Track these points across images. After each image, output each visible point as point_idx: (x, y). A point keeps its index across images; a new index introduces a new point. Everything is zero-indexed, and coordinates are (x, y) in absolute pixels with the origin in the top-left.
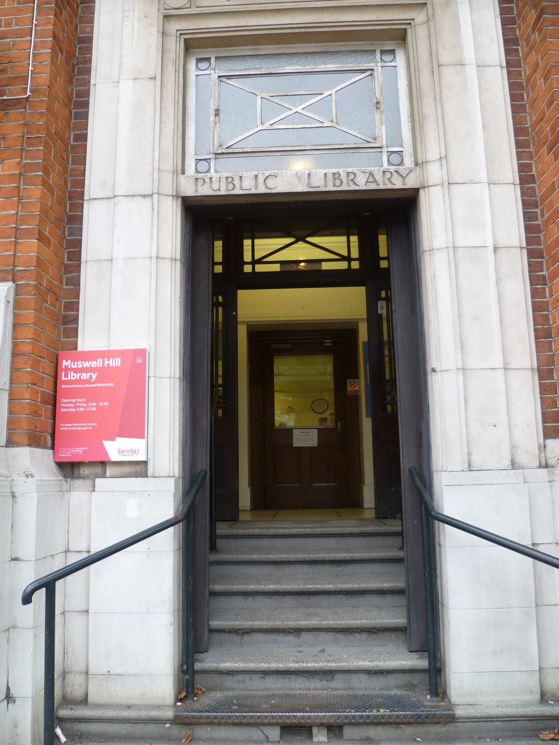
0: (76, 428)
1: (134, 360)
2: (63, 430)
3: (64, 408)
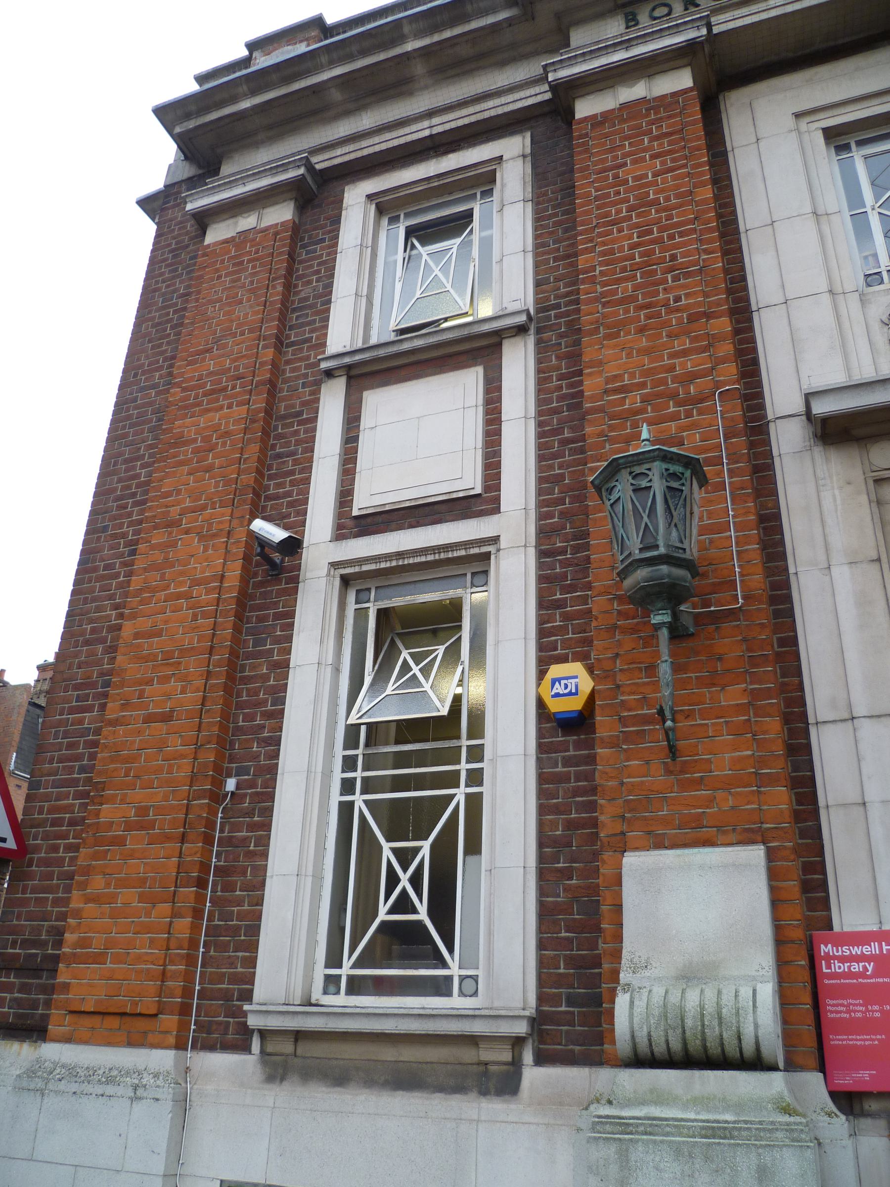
0: (855, 1042)
2: (834, 1045)
3: (832, 1012)
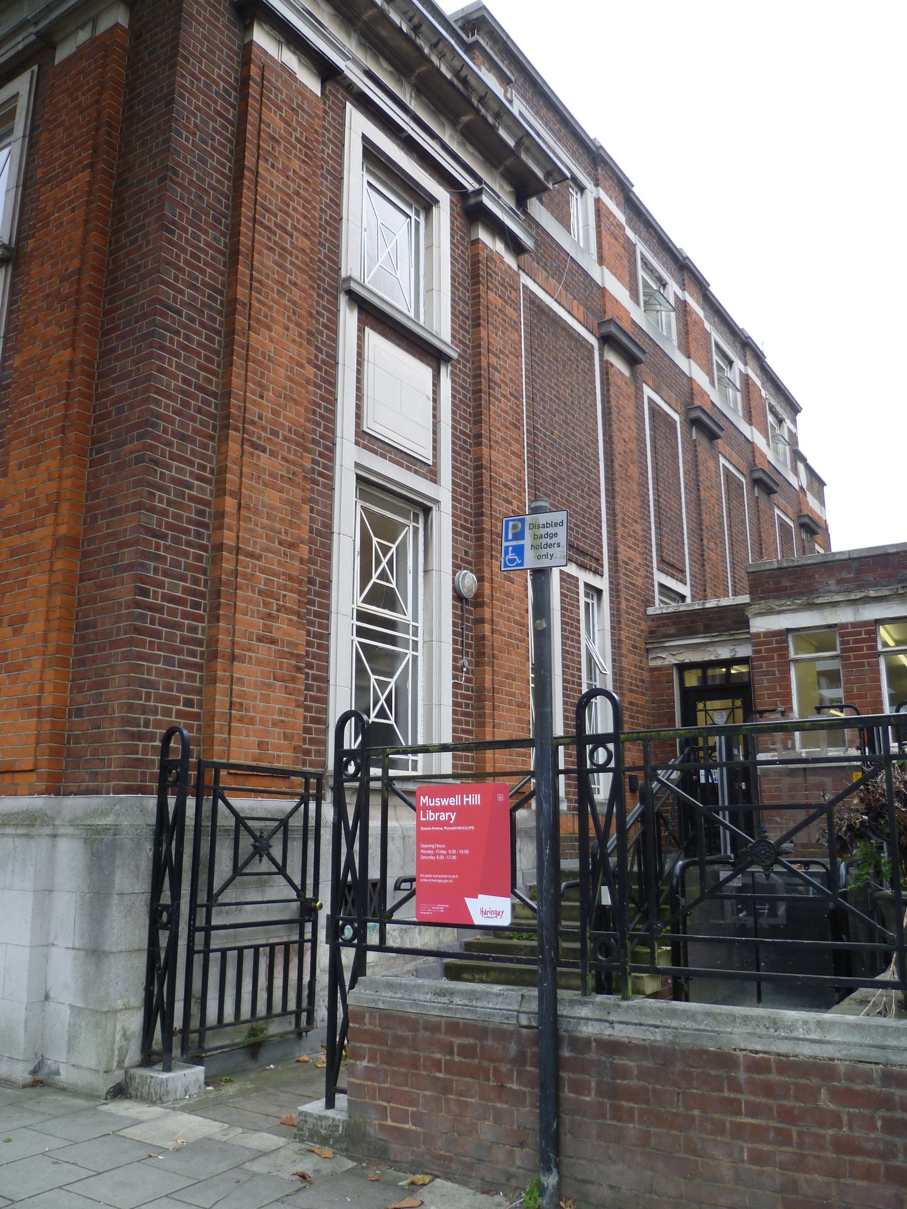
1: (495, 798)
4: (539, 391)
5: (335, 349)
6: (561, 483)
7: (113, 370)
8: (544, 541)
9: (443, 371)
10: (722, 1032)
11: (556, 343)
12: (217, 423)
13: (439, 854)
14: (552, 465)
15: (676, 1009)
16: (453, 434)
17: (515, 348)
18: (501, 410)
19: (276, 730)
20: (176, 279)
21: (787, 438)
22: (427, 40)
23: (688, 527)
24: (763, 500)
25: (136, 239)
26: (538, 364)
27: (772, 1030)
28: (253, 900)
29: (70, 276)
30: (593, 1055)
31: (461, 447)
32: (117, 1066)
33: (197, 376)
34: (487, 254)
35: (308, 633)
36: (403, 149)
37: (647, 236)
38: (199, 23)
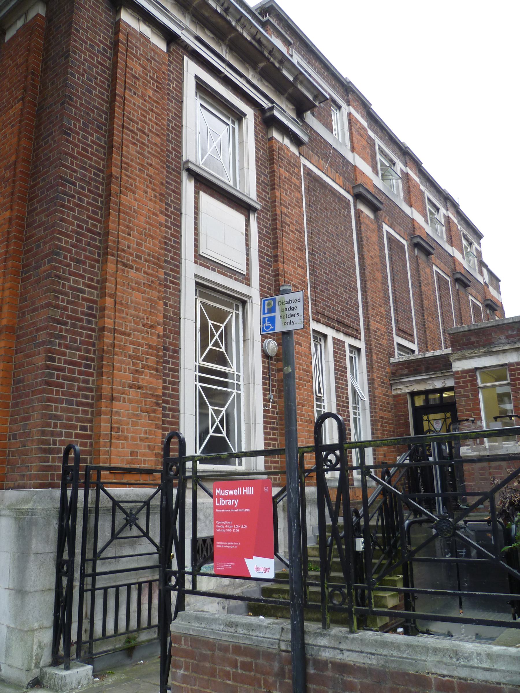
1: (263, 490)
4: (315, 228)
5: (180, 205)
6: (332, 284)
7: (35, 222)
8: (288, 313)
9: (252, 217)
10: (419, 660)
11: (325, 199)
12: (101, 252)
13: (228, 528)
14: (325, 273)
15: (386, 642)
16: (259, 255)
17: (298, 202)
18: (290, 240)
19: (143, 443)
20: (72, 163)
21: (475, 253)
22: (233, 17)
23: (414, 309)
24: (462, 291)
25: (48, 141)
26: (314, 212)
27: (455, 660)
28: (128, 554)
29: (10, 166)
30: (329, 673)
31: (265, 263)
32: (35, 667)
33: (87, 223)
34: (279, 146)
35: (165, 381)
36: (222, 84)
37: (382, 135)
38: (86, 9)
